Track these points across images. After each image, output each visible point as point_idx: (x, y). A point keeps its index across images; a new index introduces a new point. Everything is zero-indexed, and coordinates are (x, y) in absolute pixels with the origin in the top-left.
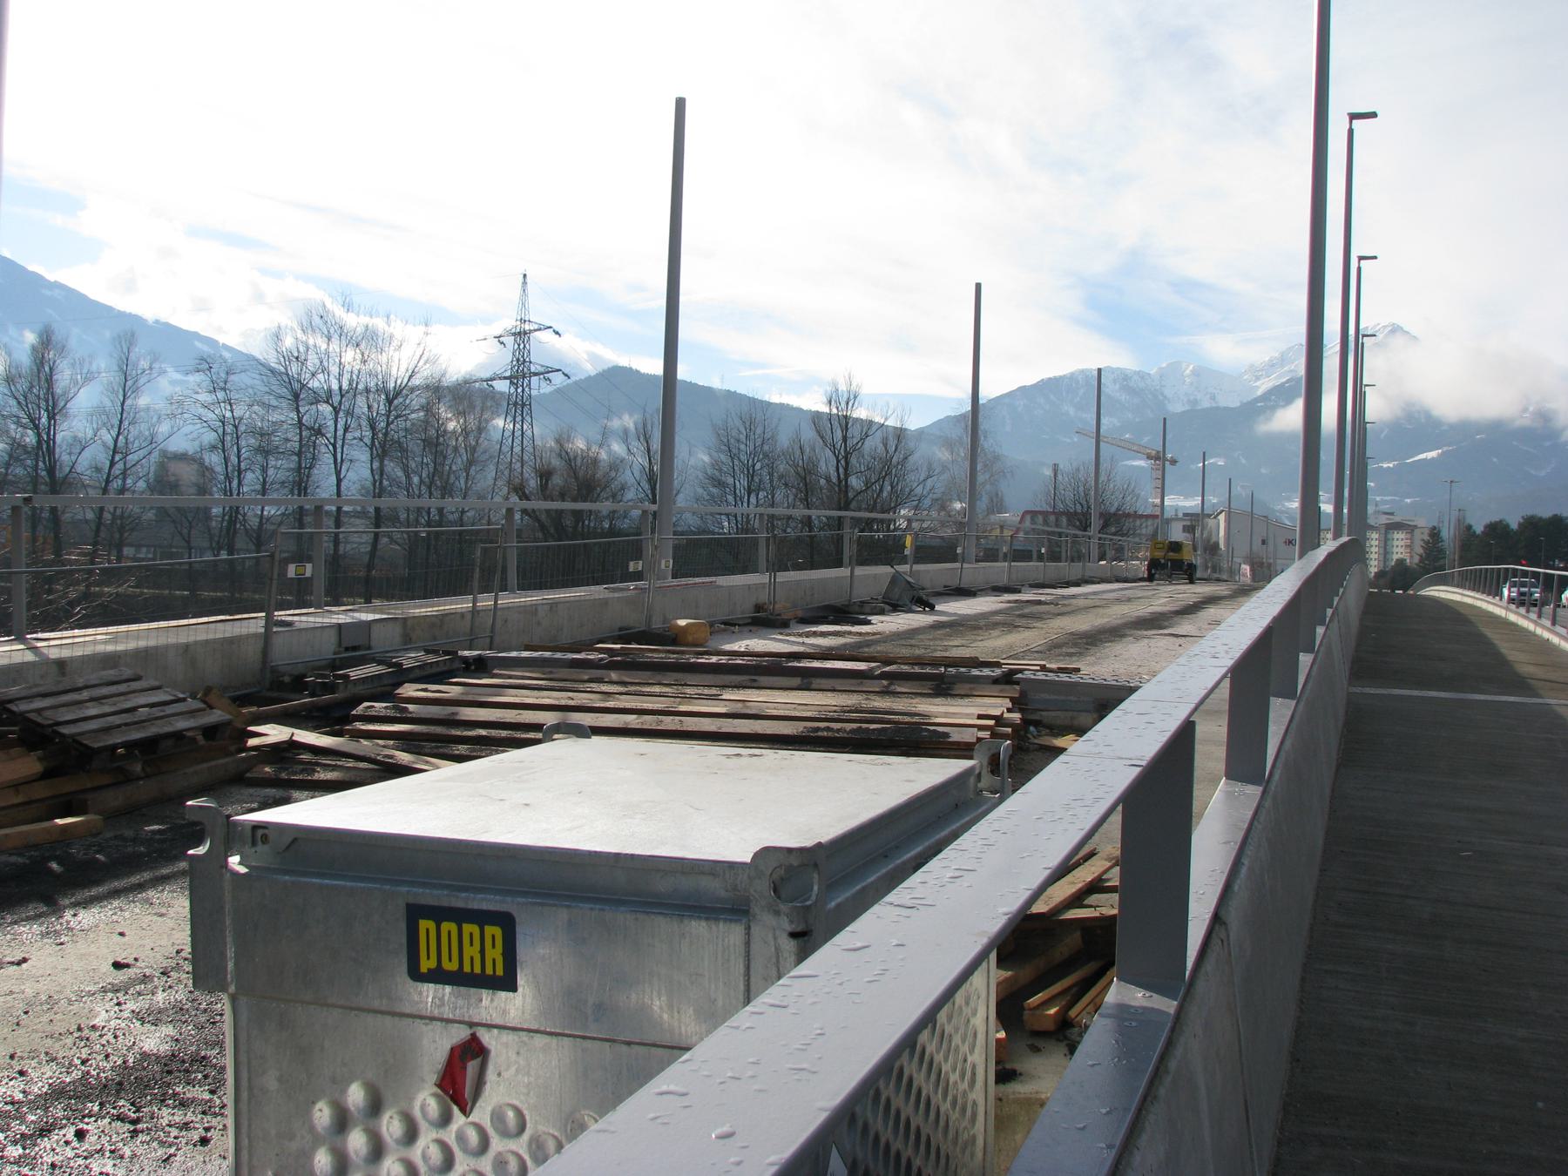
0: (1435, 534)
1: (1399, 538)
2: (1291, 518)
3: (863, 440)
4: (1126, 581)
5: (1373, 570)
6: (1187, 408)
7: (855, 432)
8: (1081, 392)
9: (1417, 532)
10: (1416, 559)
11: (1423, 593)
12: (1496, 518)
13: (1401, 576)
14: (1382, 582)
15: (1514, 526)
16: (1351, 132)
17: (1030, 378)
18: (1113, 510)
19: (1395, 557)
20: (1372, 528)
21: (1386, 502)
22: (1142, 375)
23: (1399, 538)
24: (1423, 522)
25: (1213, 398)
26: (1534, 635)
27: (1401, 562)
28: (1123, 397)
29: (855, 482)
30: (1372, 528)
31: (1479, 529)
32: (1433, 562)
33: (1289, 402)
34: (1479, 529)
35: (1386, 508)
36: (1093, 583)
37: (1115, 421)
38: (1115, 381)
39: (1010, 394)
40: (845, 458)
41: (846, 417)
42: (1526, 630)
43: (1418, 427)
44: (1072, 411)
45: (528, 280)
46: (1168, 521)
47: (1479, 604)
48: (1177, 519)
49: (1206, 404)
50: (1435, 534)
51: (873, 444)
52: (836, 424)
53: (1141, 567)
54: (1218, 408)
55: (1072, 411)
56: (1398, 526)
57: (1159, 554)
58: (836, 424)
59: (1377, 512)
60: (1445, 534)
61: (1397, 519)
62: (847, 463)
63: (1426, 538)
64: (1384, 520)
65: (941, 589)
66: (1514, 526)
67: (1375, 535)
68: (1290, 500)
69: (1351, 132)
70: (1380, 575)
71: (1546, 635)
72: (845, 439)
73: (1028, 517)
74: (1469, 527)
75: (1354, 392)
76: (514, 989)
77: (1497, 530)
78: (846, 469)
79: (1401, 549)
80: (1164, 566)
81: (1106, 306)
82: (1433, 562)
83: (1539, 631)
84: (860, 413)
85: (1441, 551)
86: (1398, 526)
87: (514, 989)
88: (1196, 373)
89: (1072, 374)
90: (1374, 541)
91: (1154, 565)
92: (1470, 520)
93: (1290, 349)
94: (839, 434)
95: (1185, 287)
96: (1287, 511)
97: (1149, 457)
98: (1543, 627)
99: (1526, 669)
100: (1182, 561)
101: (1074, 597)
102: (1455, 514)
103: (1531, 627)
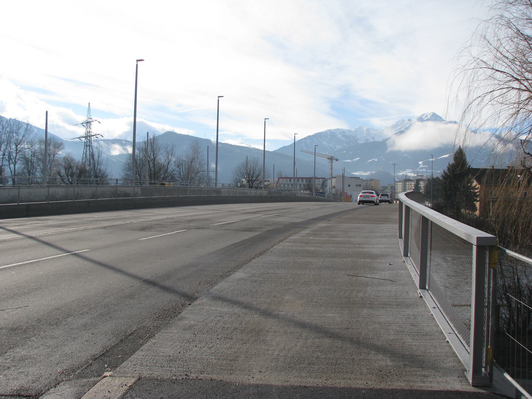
8: (329, 137)
16: (137, 65)
17: (312, 133)
25: (373, 138)
39: (305, 138)
40: (106, 177)
44: (326, 143)
45: (91, 105)
49: (371, 140)
54: (375, 142)
55: (326, 143)
69: (137, 65)
76: (477, 238)
81: (337, 108)
87: (477, 238)
88: (368, 130)
89: (326, 131)
93: (399, 121)
95: (364, 102)
97: (328, 158)
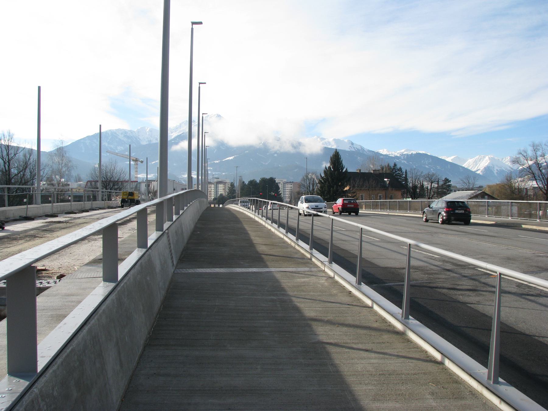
0: (232, 185)
1: (221, 187)
2: (185, 181)
3: (15, 155)
4: (112, 208)
5: (213, 198)
6: (147, 143)
7: (12, 152)
9: (227, 184)
10: (227, 194)
11: (227, 207)
12: (252, 179)
13: (221, 200)
14: (215, 201)
15: (258, 181)
18: (116, 180)
19: (220, 193)
20: (210, 183)
21: (215, 174)
22: (131, 132)
23: (221, 187)
24: (228, 181)
26: (265, 227)
27: (221, 195)
28: (125, 139)
29: (14, 171)
30: (210, 183)
31: (247, 183)
32: (231, 196)
33: (174, 139)
34: (247, 183)
35: (216, 176)
36: (96, 210)
37: (122, 148)
38: (122, 134)
39: (84, 139)
41: (8, 146)
42: (261, 225)
43: (223, 148)
46: (140, 183)
47: (245, 212)
48: (143, 182)
50: (232, 185)
51: (20, 155)
52: (4, 149)
53: (119, 201)
56: (220, 182)
57: (125, 197)
58: (4, 149)
59: (213, 178)
60: (235, 185)
61: (220, 180)
62: (9, 164)
63: (230, 186)
64: (216, 180)
65: (18, 218)
66: (258, 181)
67: (213, 186)
68: (184, 174)
70: (215, 199)
71: (269, 227)
72: (8, 155)
73: (89, 183)
74: (244, 182)
75: (201, 134)
77: (252, 183)
78: (9, 166)
79: (222, 190)
80: (127, 202)
82: (231, 196)
83: (267, 225)
84: (13, 144)
85: (235, 191)
86: (220, 182)
90: (212, 188)
91: (123, 201)
92: (244, 180)
94: (5, 153)
96: (183, 178)
98: (268, 224)
99: (261, 249)
100: (134, 199)
101: (79, 218)
102: (238, 178)
103: (264, 223)
